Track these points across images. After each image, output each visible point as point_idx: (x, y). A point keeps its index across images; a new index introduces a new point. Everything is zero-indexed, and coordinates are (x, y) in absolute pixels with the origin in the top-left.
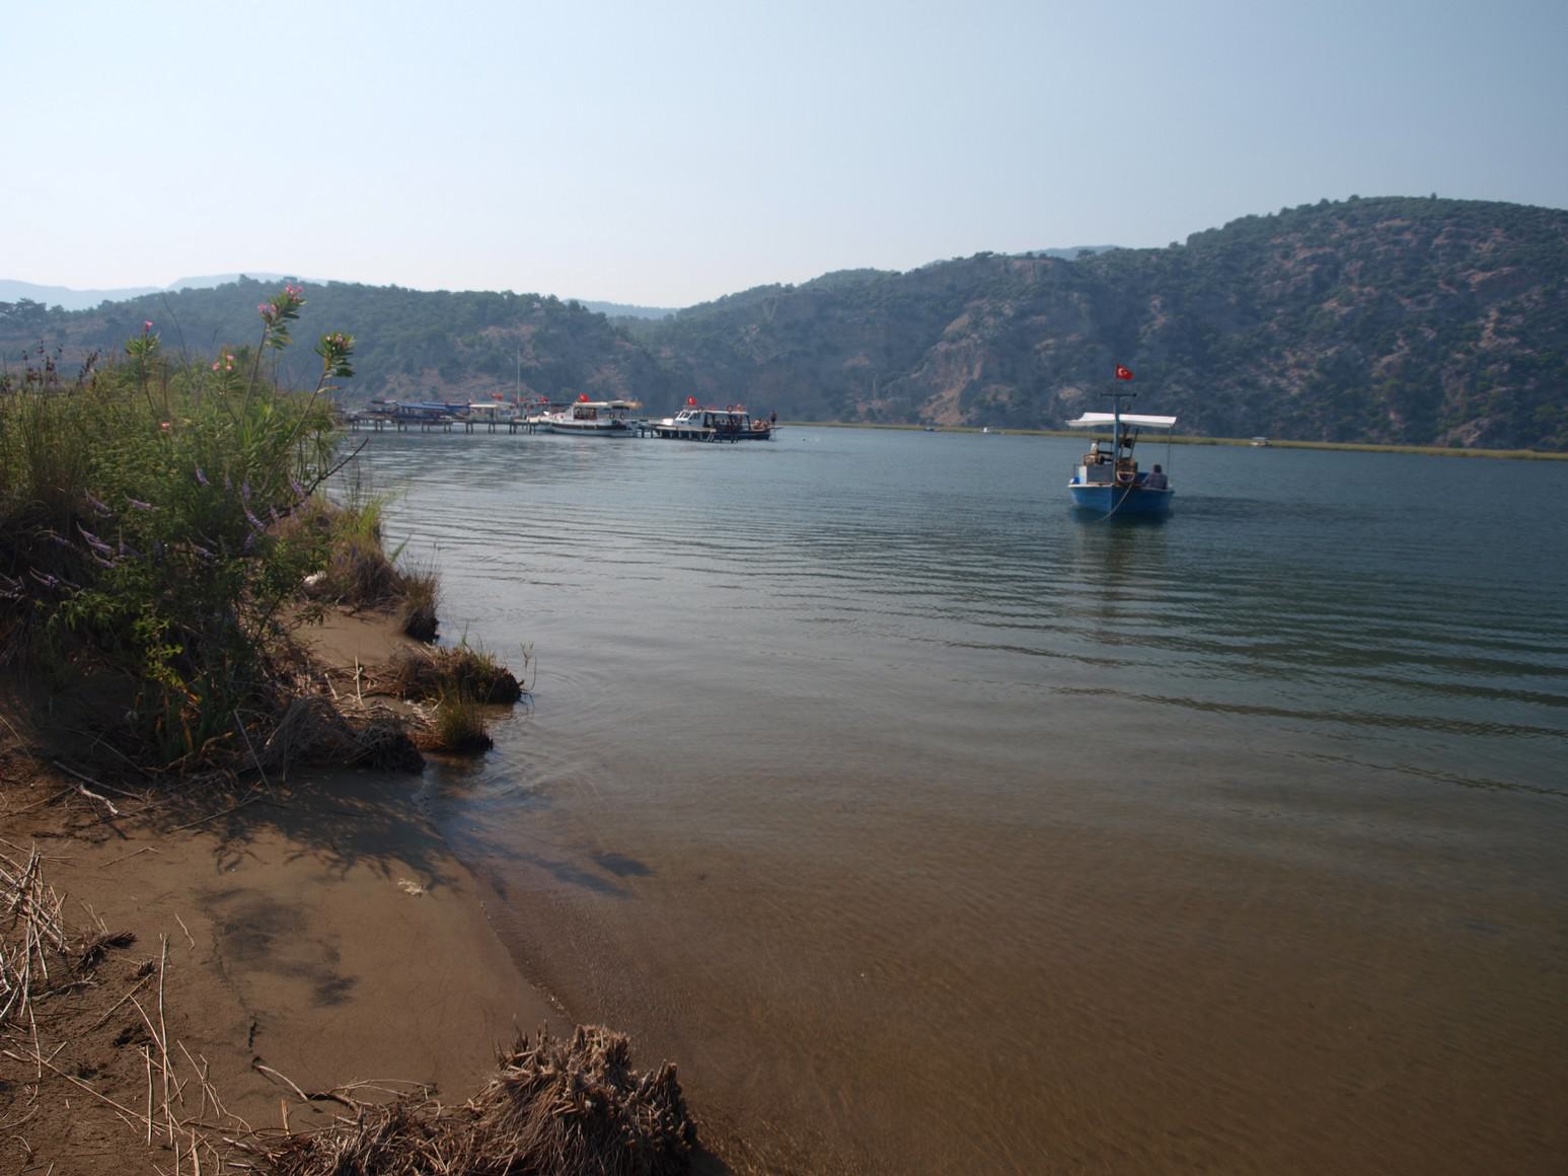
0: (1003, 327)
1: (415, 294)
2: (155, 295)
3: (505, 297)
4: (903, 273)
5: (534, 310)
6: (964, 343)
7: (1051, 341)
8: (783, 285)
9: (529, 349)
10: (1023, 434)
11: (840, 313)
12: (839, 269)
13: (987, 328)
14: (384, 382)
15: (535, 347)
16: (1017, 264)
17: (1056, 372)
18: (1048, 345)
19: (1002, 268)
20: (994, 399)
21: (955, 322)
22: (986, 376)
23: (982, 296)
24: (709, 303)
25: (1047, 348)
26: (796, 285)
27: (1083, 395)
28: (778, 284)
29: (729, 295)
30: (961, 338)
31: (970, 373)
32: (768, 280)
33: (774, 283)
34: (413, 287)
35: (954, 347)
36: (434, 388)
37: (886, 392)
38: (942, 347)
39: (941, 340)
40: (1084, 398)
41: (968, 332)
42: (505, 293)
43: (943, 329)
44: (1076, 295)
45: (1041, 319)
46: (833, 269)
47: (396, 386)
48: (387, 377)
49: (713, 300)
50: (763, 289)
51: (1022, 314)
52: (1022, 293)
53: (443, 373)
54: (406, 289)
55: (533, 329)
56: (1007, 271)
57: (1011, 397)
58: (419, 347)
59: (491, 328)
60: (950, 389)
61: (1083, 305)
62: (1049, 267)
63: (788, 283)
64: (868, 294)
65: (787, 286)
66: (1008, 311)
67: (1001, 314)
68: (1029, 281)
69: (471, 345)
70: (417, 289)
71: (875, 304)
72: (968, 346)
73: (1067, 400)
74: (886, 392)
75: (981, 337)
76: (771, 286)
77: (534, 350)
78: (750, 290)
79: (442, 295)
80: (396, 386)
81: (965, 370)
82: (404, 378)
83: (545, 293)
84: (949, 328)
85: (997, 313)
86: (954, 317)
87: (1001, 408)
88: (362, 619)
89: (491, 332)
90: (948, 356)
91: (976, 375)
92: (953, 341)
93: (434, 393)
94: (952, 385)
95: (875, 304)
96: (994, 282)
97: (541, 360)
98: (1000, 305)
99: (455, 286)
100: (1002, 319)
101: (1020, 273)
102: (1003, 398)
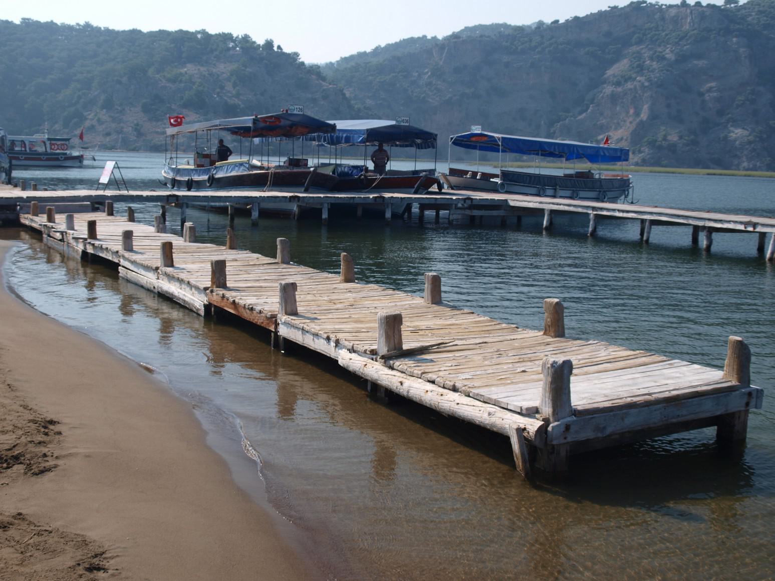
0: (668, 70)
1: (109, 32)
2: (362, 378)
3: (199, 36)
4: (619, 7)
5: (229, 49)
6: (629, 85)
7: (713, 84)
8: (429, 37)
9: (229, 87)
10: (708, 174)
11: (506, 59)
12: (477, 24)
13: (653, 71)
14: (82, 118)
15: (235, 85)
16: (673, 12)
17: (720, 113)
18: (711, 88)
19: (657, 16)
20: (665, 139)
21: (615, 66)
22: (654, 117)
23: (640, 42)
24: (365, 52)
25: (710, 90)
26: (440, 37)
27: (750, 135)
28: (425, 37)
29: (383, 45)
30: (626, 81)
31: (637, 114)
32: (416, 33)
33: (421, 35)
34: (106, 26)
35: (620, 89)
36: (137, 125)
37: (554, 133)
38: (608, 89)
39: (604, 82)
40: (751, 138)
41: (634, 76)
42: (199, 32)
43: (604, 74)
44: (735, 40)
45: (701, 63)
46: (471, 24)
47: (95, 123)
48: (85, 114)
49: (368, 50)
50: (412, 41)
51: (683, 58)
52: (682, 39)
53: (146, 109)
54: (100, 28)
55: (234, 66)
56: (663, 19)
57: (681, 137)
58: (119, 82)
59: (189, 66)
60: (616, 129)
61: (742, 50)
62: (707, 14)
63: (433, 36)
64: (531, 41)
65: (432, 38)
66: (670, 56)
67: (663, 58)
68: (687, 27)
69: (174, 80)
70: (111, 28)
71: (539, 49)
72: (635, 87)
73: (735, 140)
74: (554, 133)
75: (649, 80)
76: (419, 38)
77: (234, 87)
78: (400, 41)
79: (135, 33)
80: (95, 123)
81: (632, 111)
82: (104, 115)
83: (237, 32)
84: (610, 72)
85: (661, 58)
86: (613, 62)
87: (672, 148)
88: (85, 543)
89: (190, 69)
90: (614, 98)
91: (644, 116)
92: (618, 84)
93: (136, 130)
94: (618, 126)
95: (539, 49)
96: (650, 29)
97: (241, 97)
98: (660, 49)
99: (147, 26)
100: (665, 62)
101: (676, 20)
102: (673, 138)
